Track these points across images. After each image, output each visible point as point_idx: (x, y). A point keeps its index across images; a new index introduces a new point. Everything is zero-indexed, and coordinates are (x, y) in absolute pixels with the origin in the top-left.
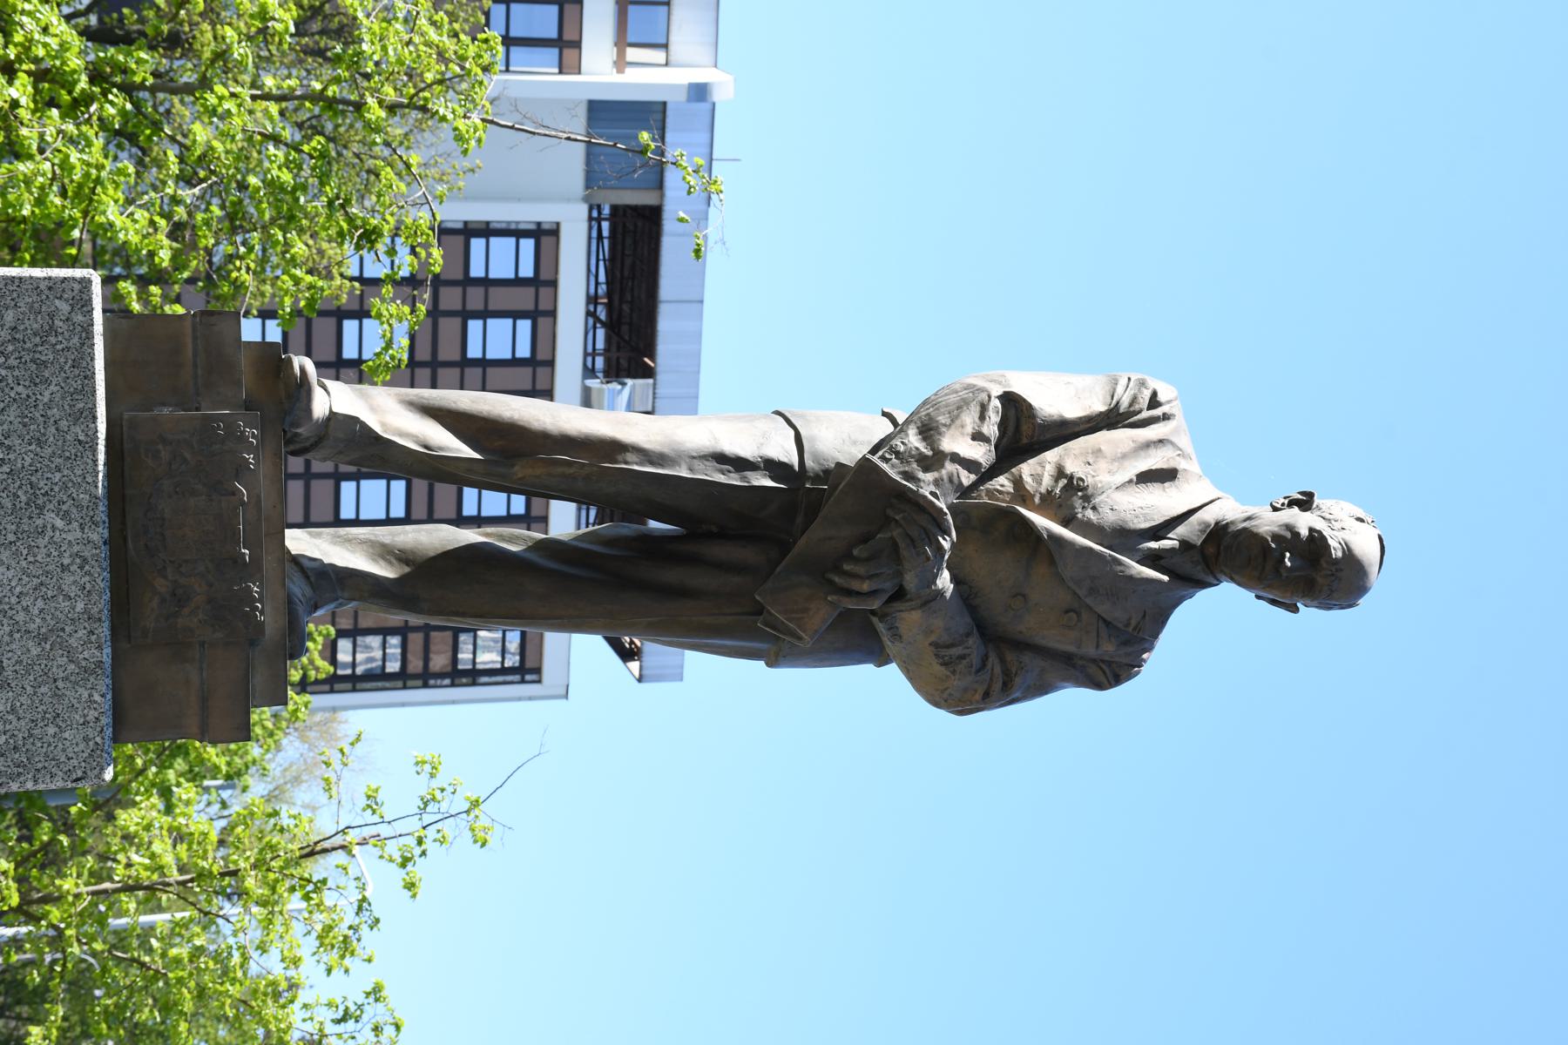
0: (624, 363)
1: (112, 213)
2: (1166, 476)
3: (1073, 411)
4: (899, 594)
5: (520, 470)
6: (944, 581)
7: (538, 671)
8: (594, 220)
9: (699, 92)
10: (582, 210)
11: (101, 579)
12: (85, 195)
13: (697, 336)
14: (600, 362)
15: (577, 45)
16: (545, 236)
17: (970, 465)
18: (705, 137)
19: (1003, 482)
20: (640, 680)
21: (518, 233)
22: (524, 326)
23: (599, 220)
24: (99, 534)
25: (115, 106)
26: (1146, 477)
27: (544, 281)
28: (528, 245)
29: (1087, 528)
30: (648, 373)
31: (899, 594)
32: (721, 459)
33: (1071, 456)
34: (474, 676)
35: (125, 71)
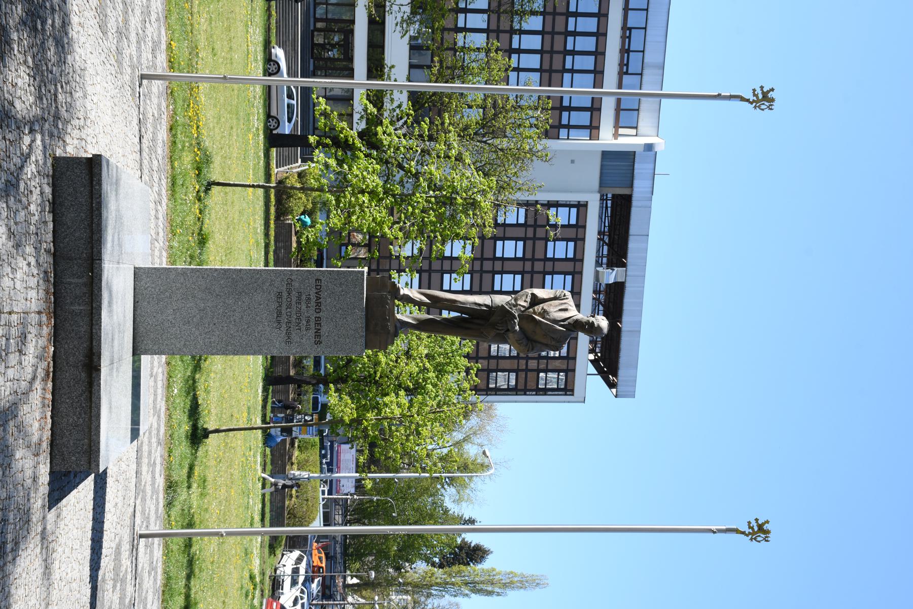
0: (614, 260)
1: (387, 230)
2: (566, 310)
3: (546, 297)
4: (508, 330)
5: (438, 305)
6: (517, 328)
7: (572, 390)
8: (603, 199)
9: (649, 147)
10: (598, 196)
11: (364, 321)
12: (381, 224)
13: (646, 250)
14: (605, 260)
15: (598, 128)
16: (581, 207)
17: (523, 307)
18: (652, 166)
19: (531, 310)
20: (616, 397)
21: (569, 206)
22: (571, 245)
23: (607, 200)
24: (364, 313)
25: (389, 200)
26: (561, 310)
27: (580, 226)
28: (574, 211)
29: (547, 319)
30: (624, 265)
31: (508, 330)
32: (476, 304)
33: (545, 306)
34: (545, 391)
35: (392, 190)
